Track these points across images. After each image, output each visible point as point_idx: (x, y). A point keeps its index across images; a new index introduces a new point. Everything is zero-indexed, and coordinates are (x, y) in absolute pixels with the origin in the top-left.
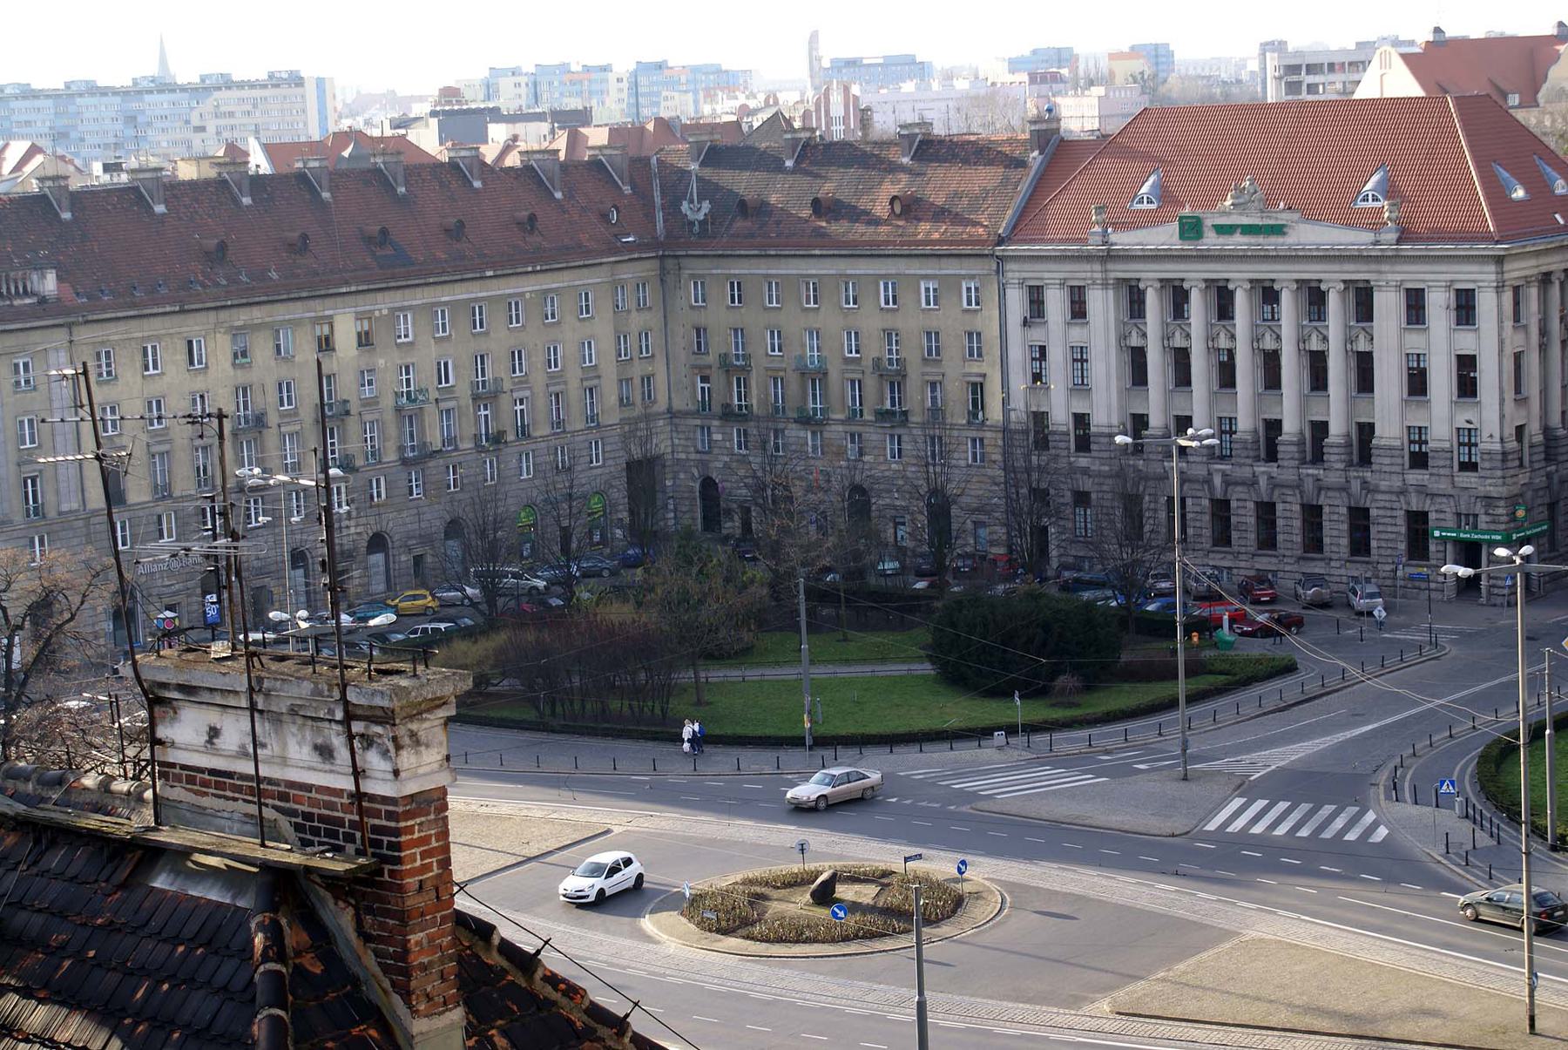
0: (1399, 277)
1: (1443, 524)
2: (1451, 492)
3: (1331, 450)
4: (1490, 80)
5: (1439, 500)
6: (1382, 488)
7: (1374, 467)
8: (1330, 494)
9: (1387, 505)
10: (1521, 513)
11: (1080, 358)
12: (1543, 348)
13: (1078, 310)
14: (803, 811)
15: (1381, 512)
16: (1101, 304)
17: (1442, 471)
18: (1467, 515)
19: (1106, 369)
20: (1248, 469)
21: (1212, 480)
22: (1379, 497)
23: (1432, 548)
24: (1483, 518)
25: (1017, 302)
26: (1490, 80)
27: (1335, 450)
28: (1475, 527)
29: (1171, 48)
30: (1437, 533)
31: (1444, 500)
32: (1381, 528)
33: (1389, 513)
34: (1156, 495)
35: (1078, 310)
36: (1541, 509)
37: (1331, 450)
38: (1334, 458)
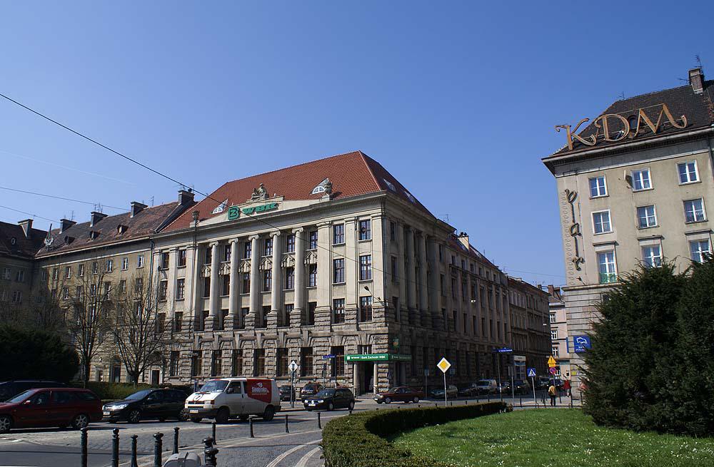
0: (331, 219)
1: (352, 352)
2: (357, 333)
3: (294, 317)
4: (341, 193)
5: (349, 338)
6: (319, 335)
7: (316, 324)
8: (292, 341)
9: (323, 344)
10: (396, 343)
11: (180, 283)
12: (407, 257)
13: (182, 262)
14: (117, 418)
15: (319, 349)
16: (191, 256)
17: (352, 322)
18: (366, 346)
19: (189, 290)
20: (253, 332)
21: (234, 340)
22: (318, 340)
23: (346, 367)
24: (374, 347)
25: (157, 258)
26: (341, 193)
27: (296, 317)
28: (370, 353)
29: (83, 217)
30: (348, 358)
31: (353, 338)
32: (318, 358)
33: (323, 349)
34: (288, 236)
35: (182, 262)
36: (407, 347)
37: (294, 317)
38: (295, 321)
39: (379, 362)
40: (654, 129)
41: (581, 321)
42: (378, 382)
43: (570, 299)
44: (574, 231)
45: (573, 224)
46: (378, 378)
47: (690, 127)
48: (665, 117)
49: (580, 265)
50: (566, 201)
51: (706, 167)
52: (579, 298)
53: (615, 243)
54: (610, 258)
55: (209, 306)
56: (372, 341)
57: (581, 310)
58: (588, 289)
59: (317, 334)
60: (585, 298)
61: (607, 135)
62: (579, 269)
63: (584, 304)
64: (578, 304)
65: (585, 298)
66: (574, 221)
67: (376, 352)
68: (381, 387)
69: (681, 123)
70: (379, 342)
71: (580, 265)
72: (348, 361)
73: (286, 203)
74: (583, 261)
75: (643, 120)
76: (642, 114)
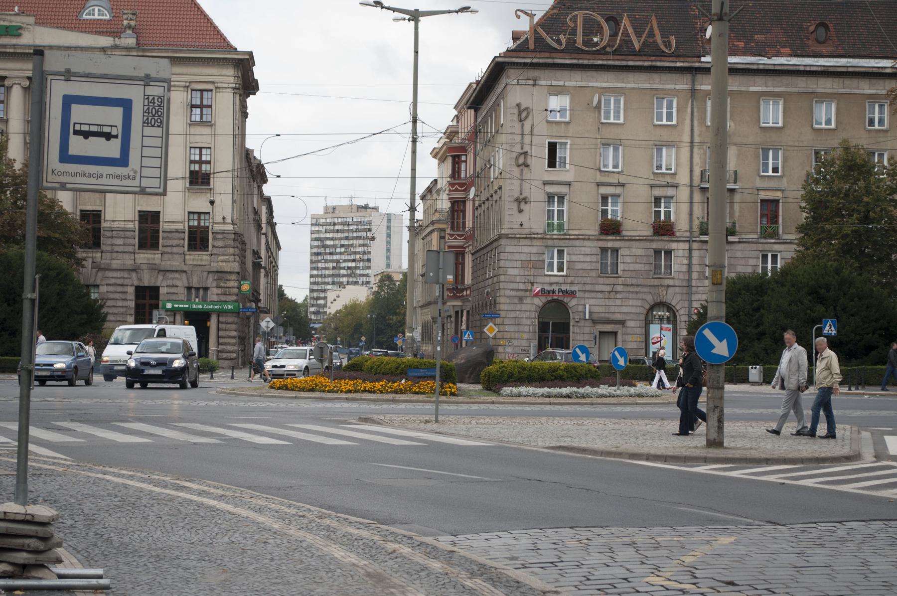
6: (114, 266)
9: (119, 281)
18: (198, 289)
22: (110, 274)
30: (169, 306)
33: (119, 289)
39: (219, 313)
40: (637, 46)
41: (518, 279)
42: (218, 344)
43: (508, 249)
44: (521, 161)
45: (521, 151)
46: (218, 337)
47: (676, 55)
48: (651, 34)
49: (523, 206)
50: (516, 118)
51: (686, 108)
52: (519, 249)
53: (569, 184)
54: (614, 203)
55: (791, 200)
56: (210, 282)
57: (519, 264)
58: (531, 239)
59: (109, 264)
60: (526, 249)
61: (579, 39)
62: (520, 211)
63: (523, 257)
64: (517, 257)
65: (526, 249)
66: (523, 124)
67: (215, 298)
68: (222, 351)
69: (668, 44)
70: (222, 284)
71: (523, 206)
72: (167, 310)
73: (39, 30)
74: (130, 385)
75: (628, 35)
76: (625, 22)
